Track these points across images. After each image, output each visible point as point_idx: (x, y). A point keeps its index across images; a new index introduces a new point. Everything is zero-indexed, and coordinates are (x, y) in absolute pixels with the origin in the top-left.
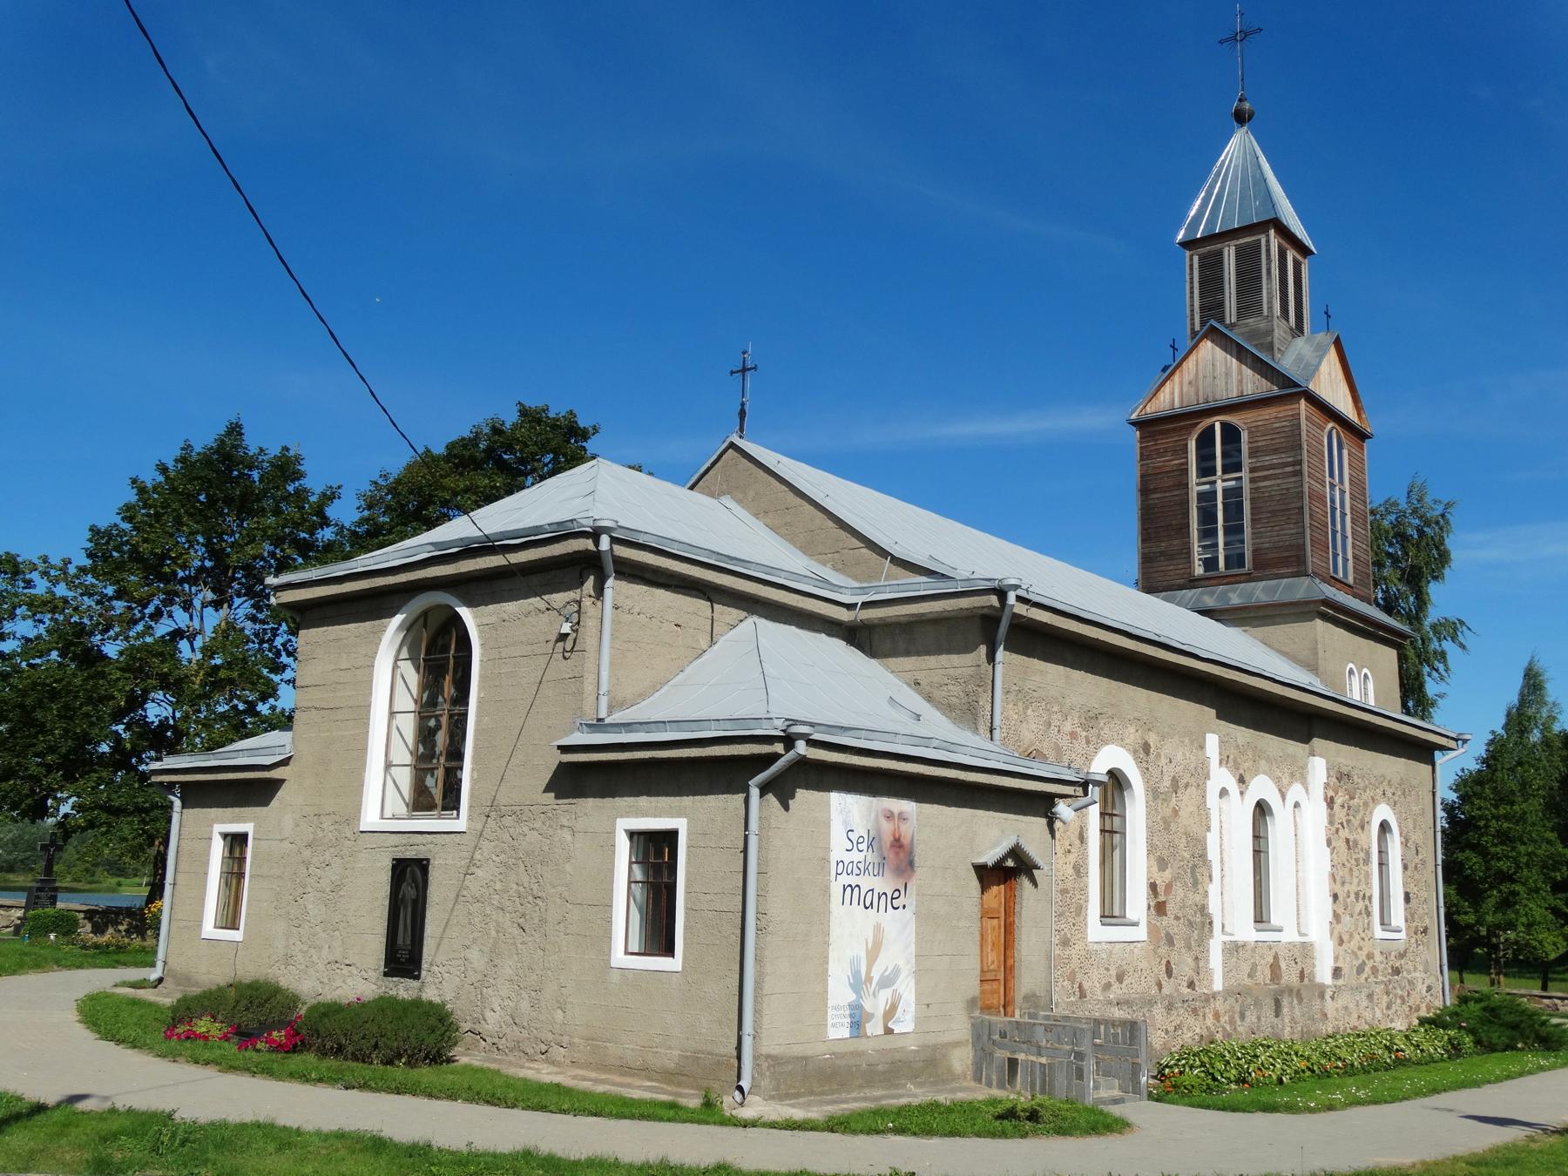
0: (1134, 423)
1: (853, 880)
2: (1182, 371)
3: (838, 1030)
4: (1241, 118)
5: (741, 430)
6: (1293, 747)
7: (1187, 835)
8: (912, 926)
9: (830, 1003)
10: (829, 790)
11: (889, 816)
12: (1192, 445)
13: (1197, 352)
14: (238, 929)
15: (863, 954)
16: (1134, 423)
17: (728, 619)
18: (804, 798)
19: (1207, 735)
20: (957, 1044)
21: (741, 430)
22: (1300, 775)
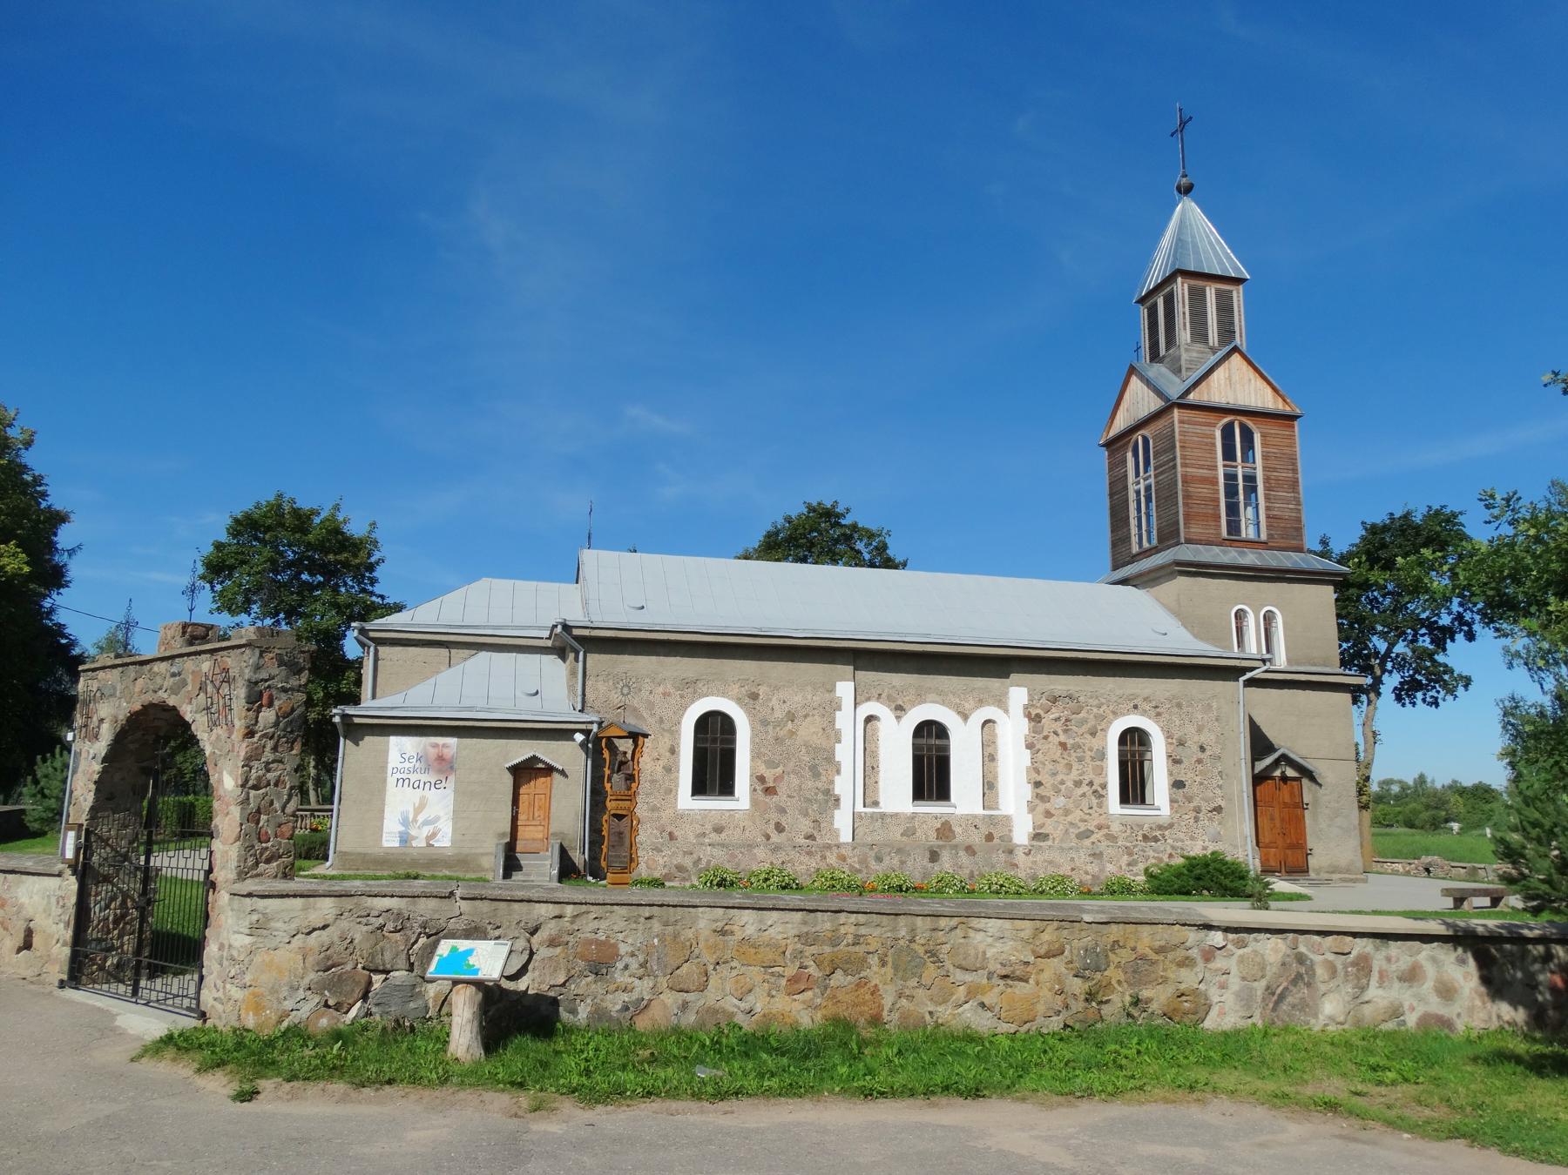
0: (1103, 446)
1: (404, 776)
2: (1208, 385)
3: (390, 841)
4: (1186, 190)
5: (589, 544)
6: (994, 683)
7: (806, 745)
8: (452, 796)
9: (385, 830)
10: (389, 735)
11: (436, 746)
12: (1218, 434)
13: (1230, 363)
14: (864, 806)
15: (411, 810)
16: (1103, 446)
17: (463, 655)
18: (369, 741)
19: (838, 684)
20: (487, 854)
21: (589, 544)
22: (1001, 702)
